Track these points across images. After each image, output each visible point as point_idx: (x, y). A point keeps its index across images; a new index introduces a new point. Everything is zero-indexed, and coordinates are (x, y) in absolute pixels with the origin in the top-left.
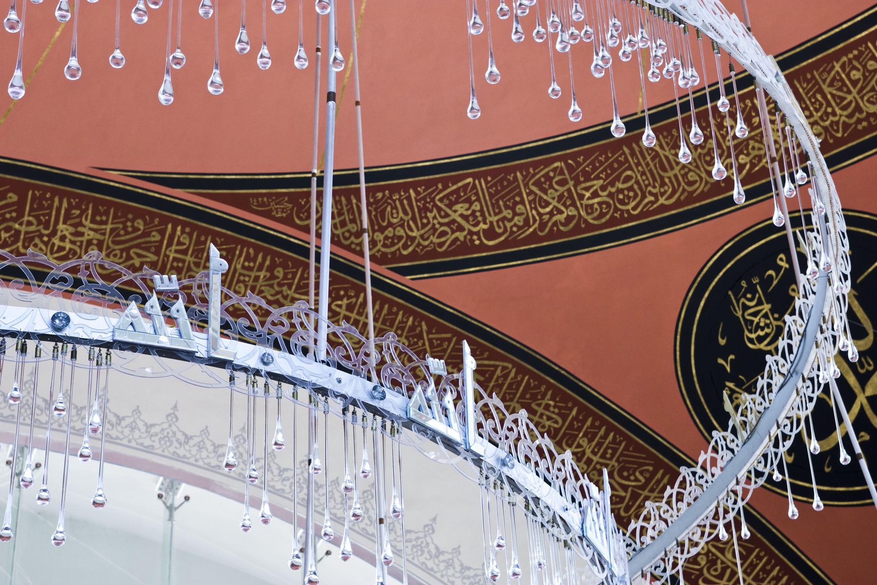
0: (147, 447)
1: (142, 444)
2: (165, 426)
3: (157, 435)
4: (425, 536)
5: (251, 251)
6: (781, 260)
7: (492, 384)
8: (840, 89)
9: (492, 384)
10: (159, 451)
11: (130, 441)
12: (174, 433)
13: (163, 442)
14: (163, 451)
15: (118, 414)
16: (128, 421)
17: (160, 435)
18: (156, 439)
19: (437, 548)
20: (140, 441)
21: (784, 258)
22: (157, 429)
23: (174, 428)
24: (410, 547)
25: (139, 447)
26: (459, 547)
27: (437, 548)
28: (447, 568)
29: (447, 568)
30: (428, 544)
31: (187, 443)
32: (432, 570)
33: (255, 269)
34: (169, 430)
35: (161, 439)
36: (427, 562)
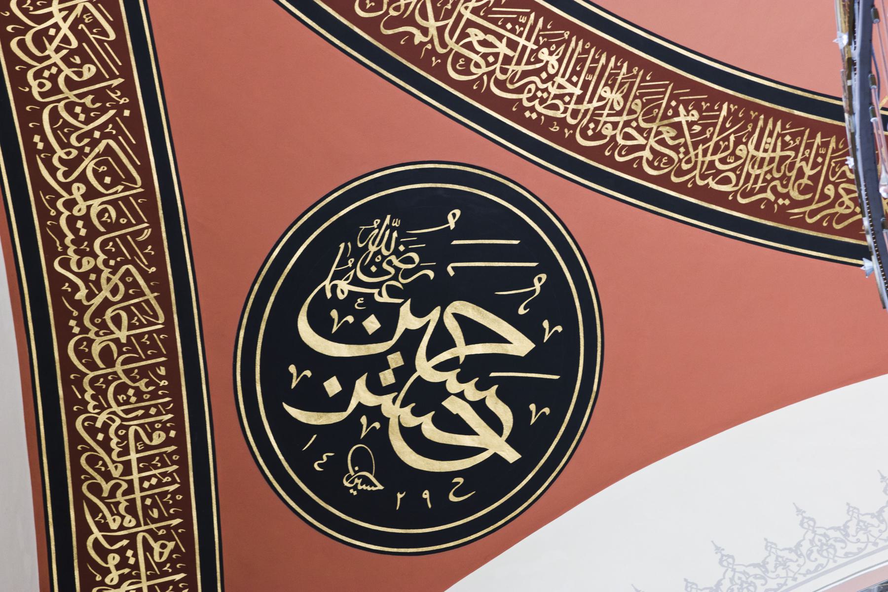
0: (816, 570)
1: (808, 572)
2: (810, 535)
3: (812, 552)
4: (734, 570)
5: (147, 233)
6: (540, 280)
7: (153, 526)
8: (51, 39)
9: (153, 526)
10: (831, 565)
11: (795, 579)
12: (825, 535)
13: (825, 553)
14: (835, 562)
15: (756, 562)
16: (771, 561)
17: (815, 549)
18: (815, 555)
19: (755, 565)
20: (803, 570)
21: (543, 281)
22: (806, 545)
23: (819, 531)
24: (818, 556)
25: (809, 576)
26: (686, 580)
27: (755, 565)
28: (786, 567)
29: (786, 567)
30: (744, 573)
31: (847, 535)
32: (860, 550)
33: (145, 298)
34: (817, 537)
35: (819, 552)
36: (846, 550)
